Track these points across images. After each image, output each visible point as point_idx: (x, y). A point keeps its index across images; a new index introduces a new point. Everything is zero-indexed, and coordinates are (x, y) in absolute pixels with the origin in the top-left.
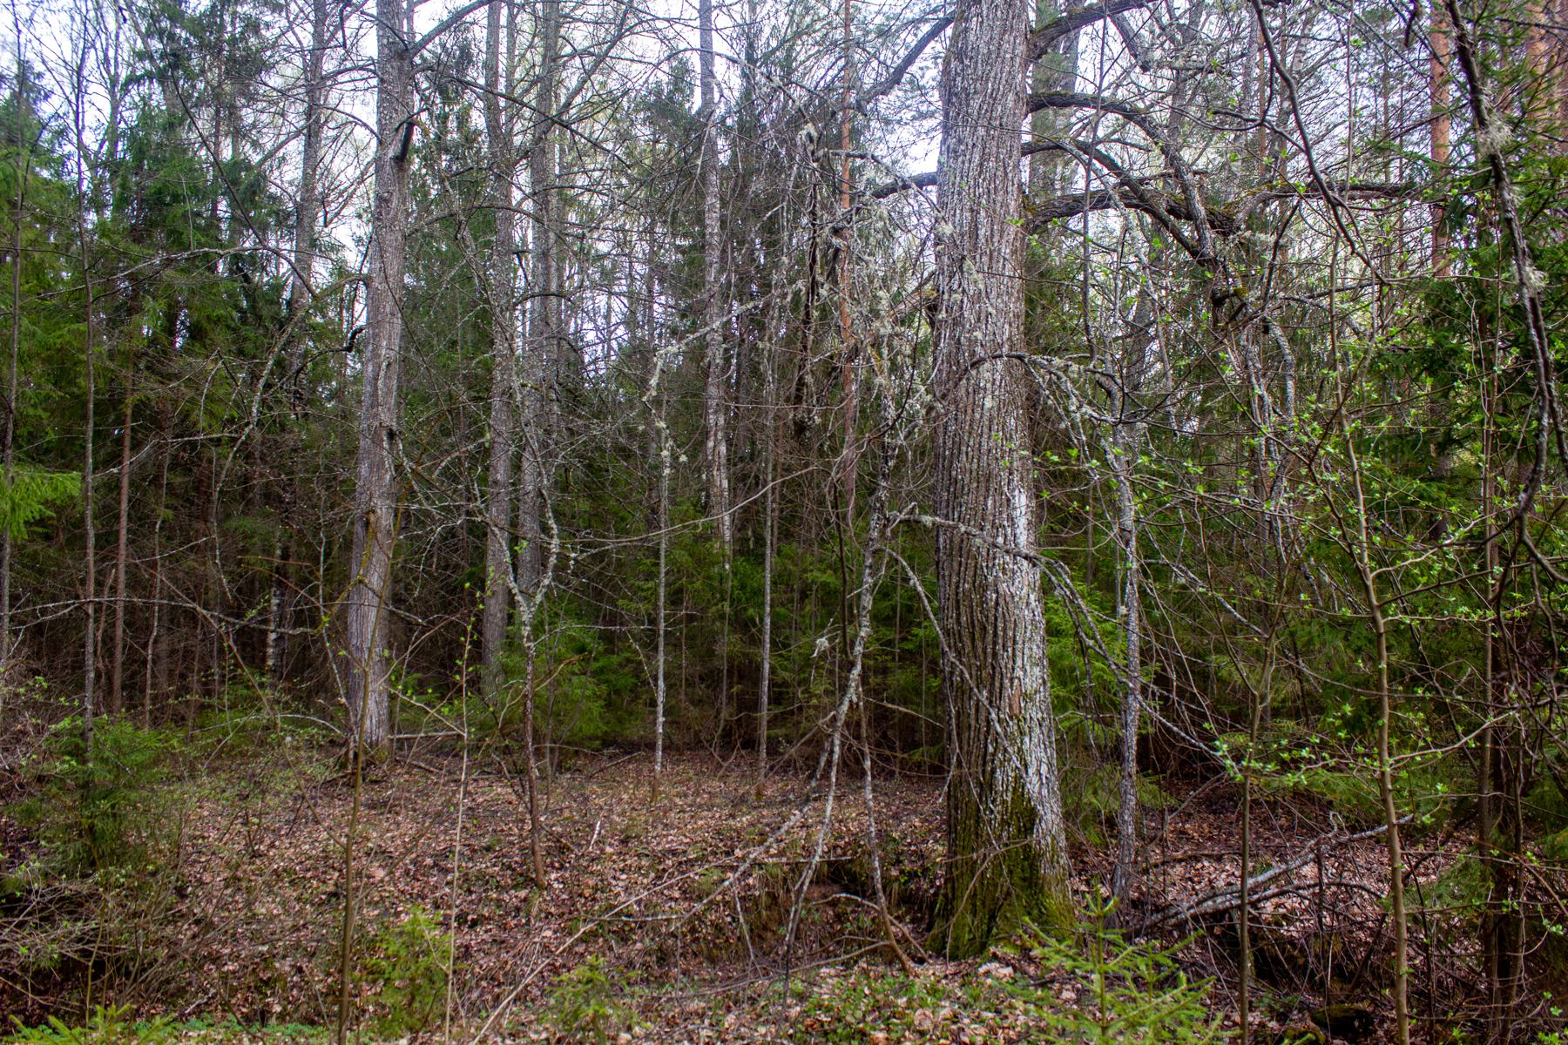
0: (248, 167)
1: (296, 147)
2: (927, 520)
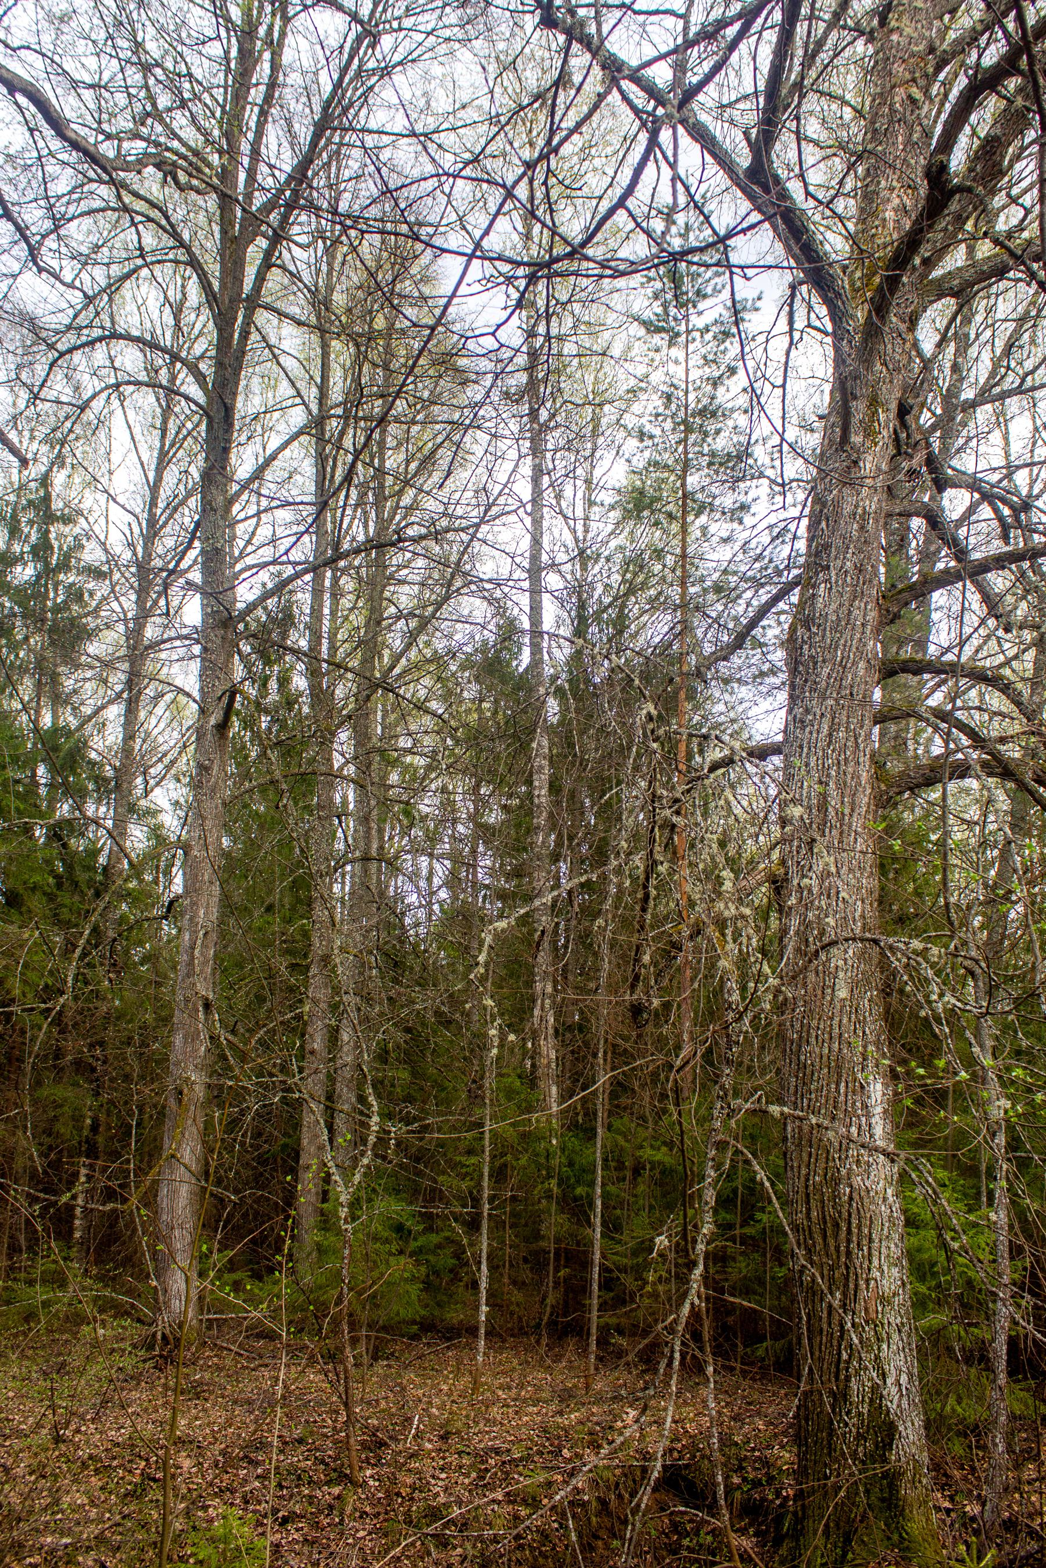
0: (69, 733)
1: (114, 712)
2: (775, 1109)
